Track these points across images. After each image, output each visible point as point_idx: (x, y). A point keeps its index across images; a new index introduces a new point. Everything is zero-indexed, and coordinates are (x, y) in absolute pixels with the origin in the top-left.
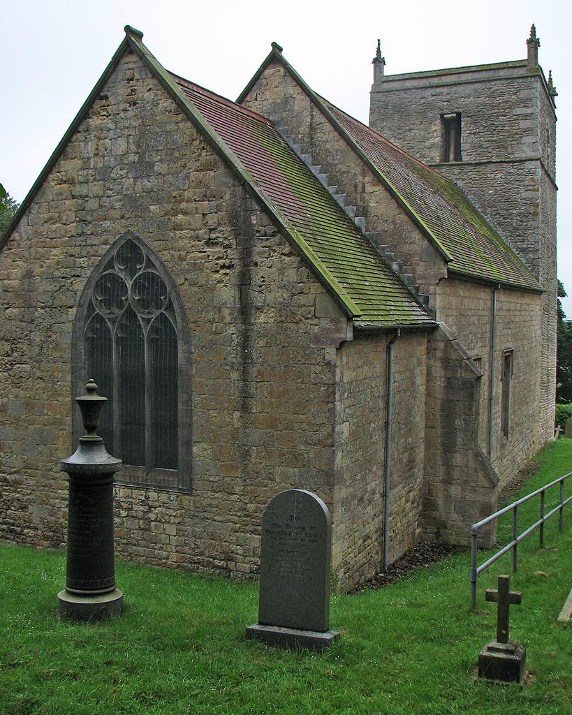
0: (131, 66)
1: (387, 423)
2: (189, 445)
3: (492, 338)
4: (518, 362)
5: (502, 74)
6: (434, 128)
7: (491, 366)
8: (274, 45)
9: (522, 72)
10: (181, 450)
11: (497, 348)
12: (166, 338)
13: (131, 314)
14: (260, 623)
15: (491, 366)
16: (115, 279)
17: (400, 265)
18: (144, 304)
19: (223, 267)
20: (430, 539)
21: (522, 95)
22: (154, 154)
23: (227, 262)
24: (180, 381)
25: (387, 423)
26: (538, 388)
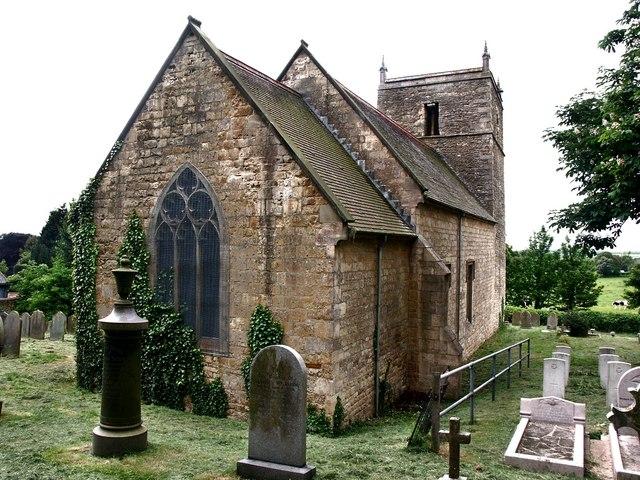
0: (191, 44)
1: (377, 306)
2: (227, 320)
3: (459, 251)
4: (479, 271)
5: (465, 76)
6: (420, 113)
7: (459, 270)
8: (303, 42)
9: (479, 76)
10: (222, 323)
11: (463, 259)
12: (211, 241)
13: (188, 224)
14: (250, 458)
15: (459, 270)
16: (177, 197)
17: (390, 194)
18: (195, 215)
19: (253, 186)
20: (397, 383)
21: (480, 90)
22: (206, 105)
23: (256, 183)
24: (222, 270)
25: (377, 306)
26: (493, 290)
